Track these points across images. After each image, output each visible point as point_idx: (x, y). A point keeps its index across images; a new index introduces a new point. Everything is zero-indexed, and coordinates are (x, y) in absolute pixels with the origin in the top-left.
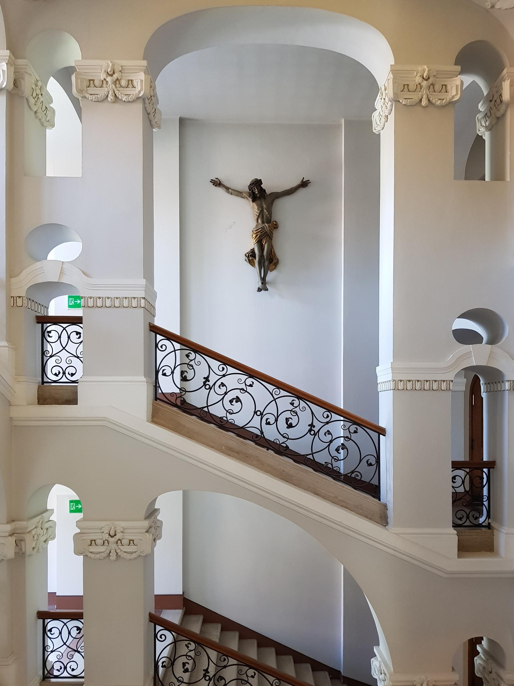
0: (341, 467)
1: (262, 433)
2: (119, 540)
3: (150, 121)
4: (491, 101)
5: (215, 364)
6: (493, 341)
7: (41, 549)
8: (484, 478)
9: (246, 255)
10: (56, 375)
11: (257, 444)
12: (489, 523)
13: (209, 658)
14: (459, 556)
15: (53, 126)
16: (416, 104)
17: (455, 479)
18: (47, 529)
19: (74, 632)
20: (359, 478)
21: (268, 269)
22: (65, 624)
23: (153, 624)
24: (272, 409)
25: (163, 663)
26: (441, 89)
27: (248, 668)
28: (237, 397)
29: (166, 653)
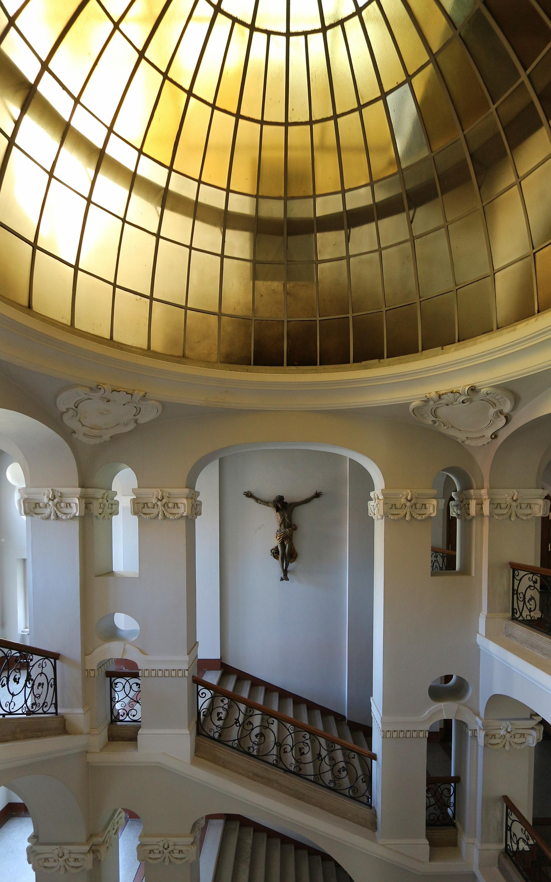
13: (239, 710)
16: (402, 519)
22: (127, 681)
25: (204, 712)
26: (422, 507)
29: (205, 706)
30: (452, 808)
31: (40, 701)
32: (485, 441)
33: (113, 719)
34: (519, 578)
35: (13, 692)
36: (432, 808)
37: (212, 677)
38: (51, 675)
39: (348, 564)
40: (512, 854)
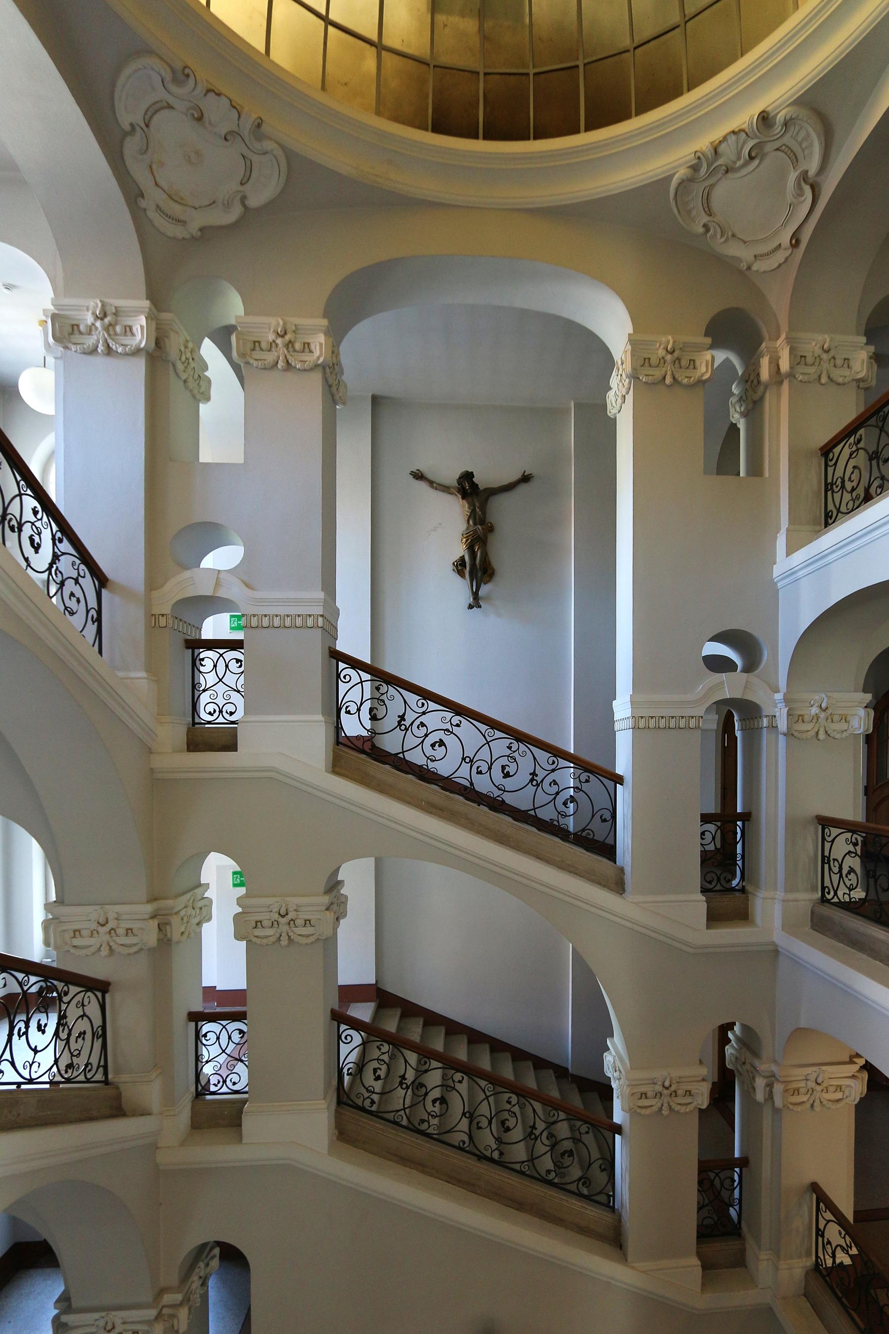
0: (571, 824)
1: (472, 784)
2: (292, 920)
3: (333, 396)
4: (747, 381)
5: (412, 698)
6: (749, 668)
7: (193, 934)
8: (737, 833)
9: (454, 563)
10: (210, 713)
11: (467, 799)
12: (743, 887)
13: (406, 1061)
14: (708, 927)
15: (208, 399)
16: (660, 381)
17: (704, 835)
18: (201, 908)
19: (236, 1037)
20: (591, 837)
21: (481, 581)
22: (224, 1027)
23: (336, 1023)
24: (484, 754)
25: (349, 1070)
27: (455, 1071)
28: (440, 739)
29: (353, 1057)
30: (737, 1208)
31: (81, 1061)
32: (780, 257)
33: (199, 1090)
34: (830, 839)
35: (36, 1047)
36: (705, 1210)
37: (363, 1012)
38: (97, 1022)
39: (573, 470)
40: (825, 1273)
